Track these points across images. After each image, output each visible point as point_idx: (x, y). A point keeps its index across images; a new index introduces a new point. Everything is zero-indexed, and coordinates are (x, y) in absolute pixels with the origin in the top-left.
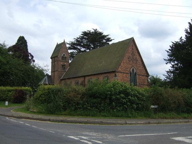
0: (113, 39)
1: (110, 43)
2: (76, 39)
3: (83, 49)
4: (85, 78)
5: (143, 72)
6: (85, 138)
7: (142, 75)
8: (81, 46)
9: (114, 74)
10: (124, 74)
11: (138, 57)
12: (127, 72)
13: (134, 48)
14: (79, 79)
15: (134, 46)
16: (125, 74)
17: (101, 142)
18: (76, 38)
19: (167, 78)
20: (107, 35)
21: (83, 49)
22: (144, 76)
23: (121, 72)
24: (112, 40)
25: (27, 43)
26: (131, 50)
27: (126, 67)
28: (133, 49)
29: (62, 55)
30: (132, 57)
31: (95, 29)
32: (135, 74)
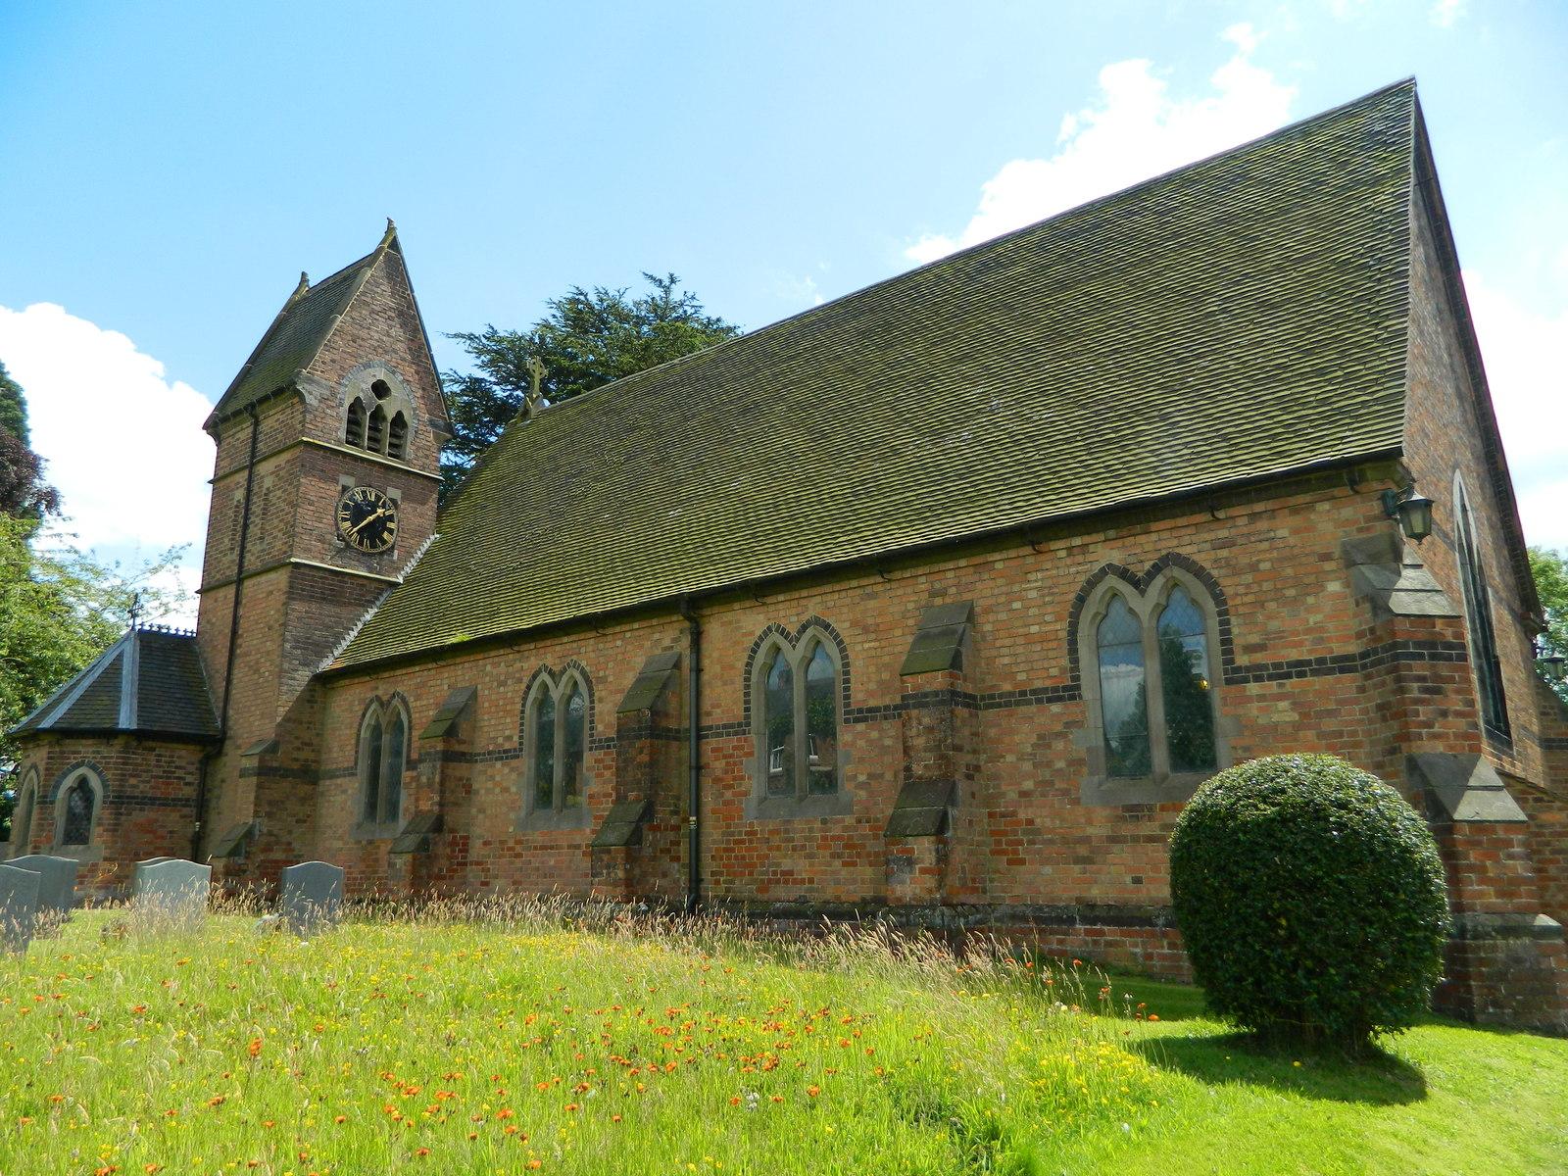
29: (360, 386)
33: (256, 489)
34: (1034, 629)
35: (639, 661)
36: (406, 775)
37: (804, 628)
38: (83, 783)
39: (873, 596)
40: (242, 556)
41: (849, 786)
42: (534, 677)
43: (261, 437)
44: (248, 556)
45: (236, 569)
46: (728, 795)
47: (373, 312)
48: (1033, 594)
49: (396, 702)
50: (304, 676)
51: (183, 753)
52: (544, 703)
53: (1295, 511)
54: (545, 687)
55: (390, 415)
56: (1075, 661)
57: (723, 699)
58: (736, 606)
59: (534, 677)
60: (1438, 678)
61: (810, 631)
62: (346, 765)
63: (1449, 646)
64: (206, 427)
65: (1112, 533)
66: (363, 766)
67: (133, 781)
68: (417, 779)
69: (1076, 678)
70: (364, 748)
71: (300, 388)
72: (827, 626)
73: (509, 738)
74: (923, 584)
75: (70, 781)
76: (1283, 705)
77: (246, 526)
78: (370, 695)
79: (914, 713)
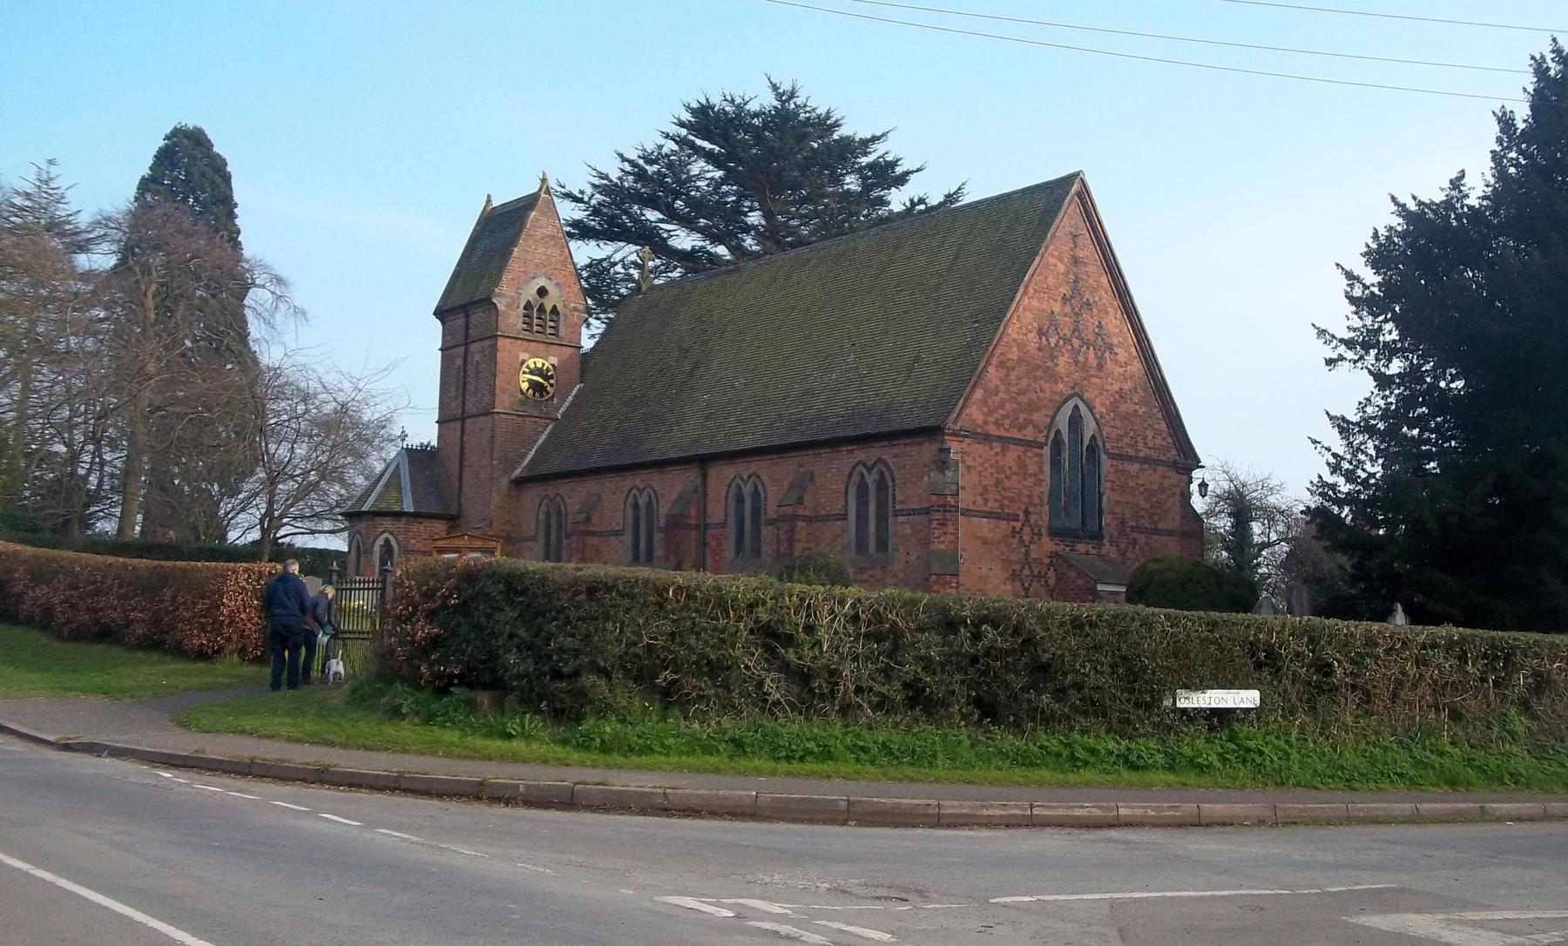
0: (918, 170)
1: (897, 200)
2: (632, 163)
3: (684, 240)
4: (705, 477)
5: (1150, 434)
6: (776, 908)
7: (1146, 460)
8: (672, 216)
9: (935, 447)
10: (1004, 451)
11: (1114, 322)
12: (1029, 433)
13: (1087, 251)
14: (655, 479)
15: (1086, 239)
16: (1013, 453)
17: (886, 937)
18: (633, 155)
19: (1335, 469)
20: (874, 139)
21: (684, 240)
22: (1158, 462)
23: (986, 438)
24: (908, 173)
25: (227, 178)
26: (1061, 268)
27: (1024, 399)
28: (1076, 261)
29: (530, 293)
30: (1066, 324)
31: (786, 87)
32: (1092, 448)
33: (469, 361)
34: (834, 487)
35: (679, 487)
36: (565, 542)
37: (750, 477)
38: (387, 541)
39: (776, 464)
40: (464, 403)
41: (765, 555)
42: (630, 491)
43: (471, 325)
44: (467, 403)
45: (460, 411)
46: (717, 558)
47: (535, 240)
48: (834, 470)
49: (558, 499)
50: (505, 481)
51: (437, 525)
52: (636, 506)
53: (918, 444)
54: (635, 497)
55: (548, 308)
56: (847, 503)
57: (717, 509)
58: (722, 462)
59: (630, 491)
60: (944, 519)
61: (752, 479)
62: (531, 534)
63: (953, 506)
64: (435, 314)
65: (861, 446)
66: (541, 536)
67: (413, 541)
68: (570, 544)
69: (846, 510)
70: (542, 527)
71: (494, 301)
72: (759, 477)
73: (618, 524)
74: (796, 460)
75: (380, 541)
76: (908, 527)
77: (464, 386)
78: (543, 494)
79: (782, 524)
